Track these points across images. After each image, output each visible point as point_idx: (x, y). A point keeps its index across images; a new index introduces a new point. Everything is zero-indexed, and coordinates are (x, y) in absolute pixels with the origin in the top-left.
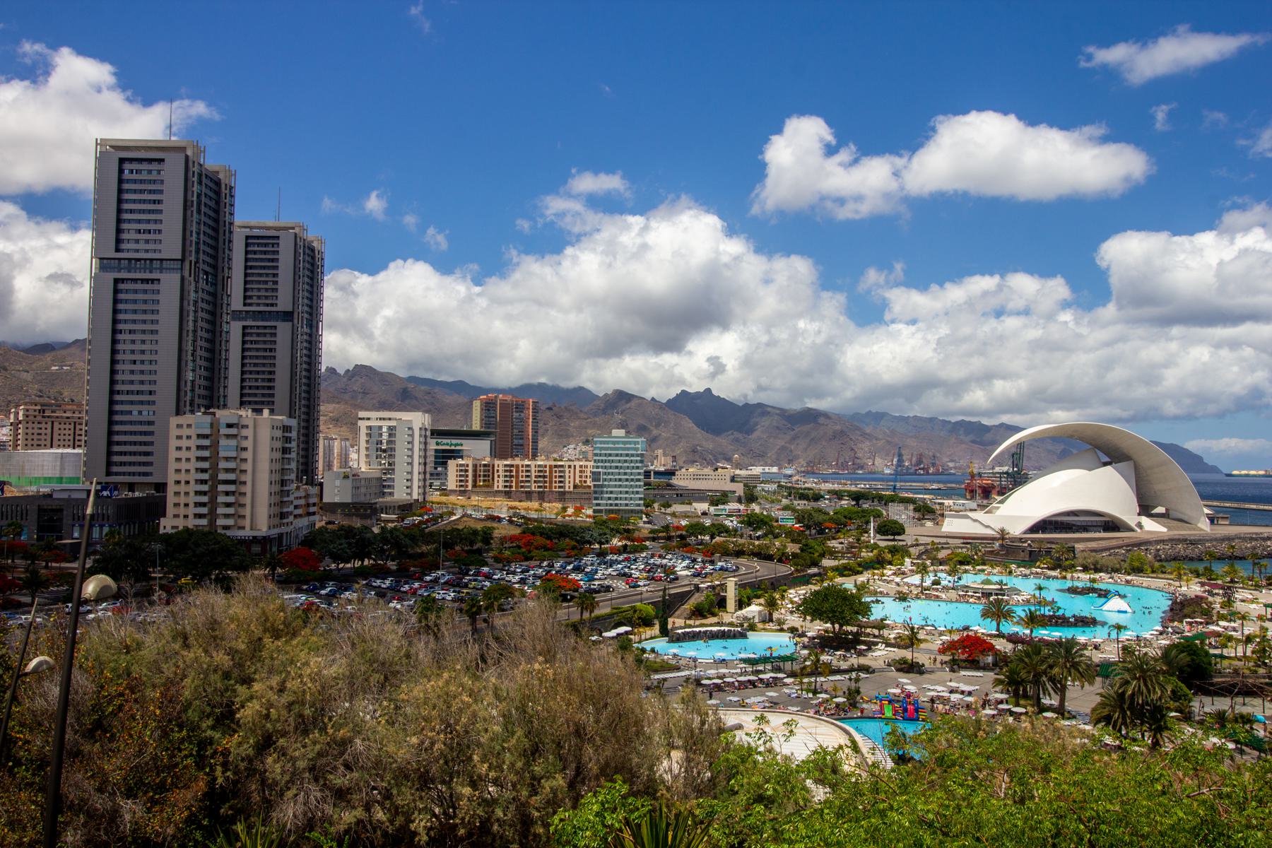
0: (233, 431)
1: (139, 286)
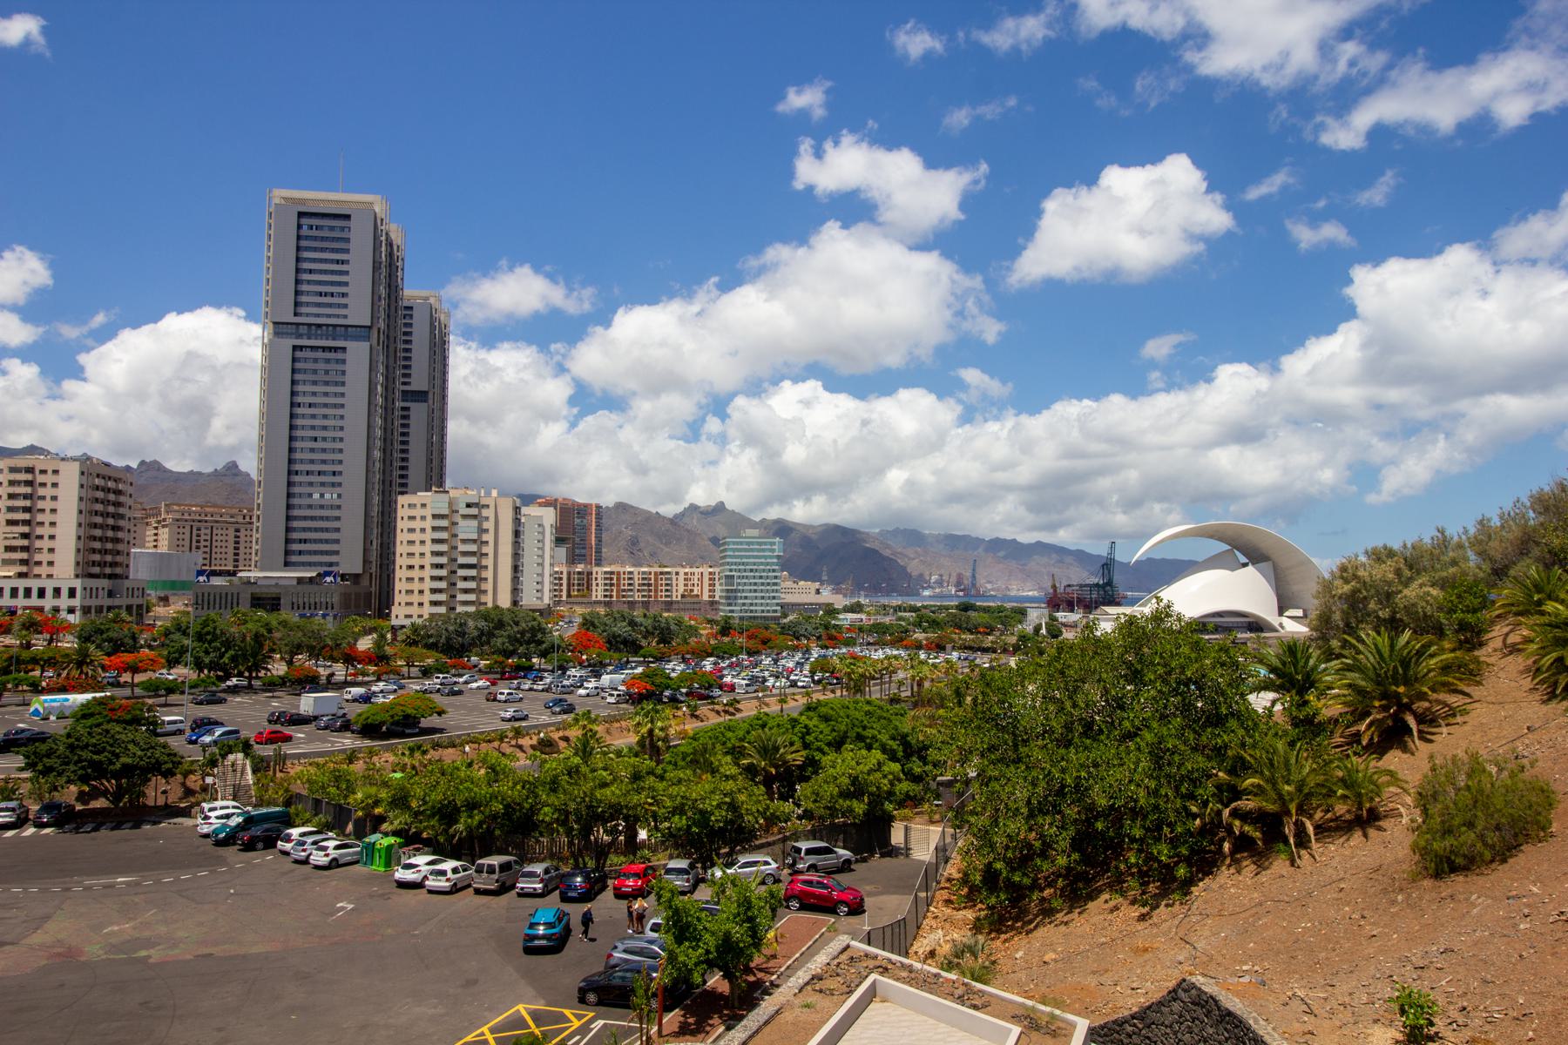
0: (474, 511)
1: (320, 354)
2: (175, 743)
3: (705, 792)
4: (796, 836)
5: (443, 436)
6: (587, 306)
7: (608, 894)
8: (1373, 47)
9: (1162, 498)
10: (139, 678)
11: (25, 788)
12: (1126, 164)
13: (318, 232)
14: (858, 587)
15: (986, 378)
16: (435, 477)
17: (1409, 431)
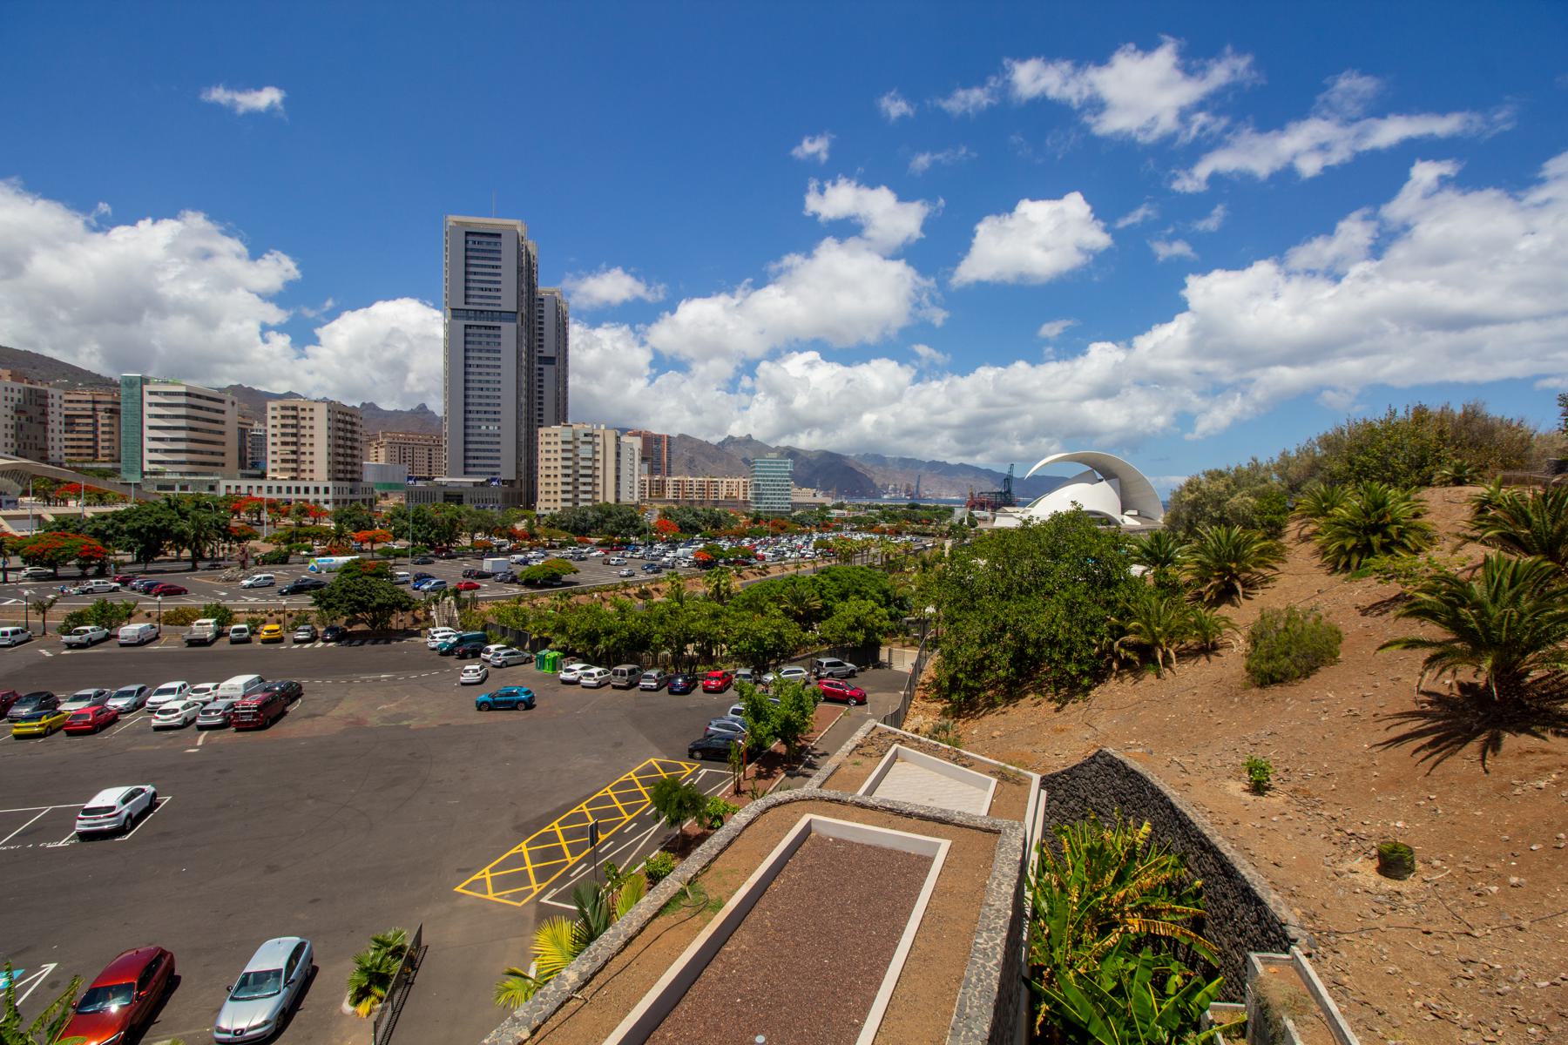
1: (483, 331)
2: (407, 588)
3: (763, 626)
4: (818, 655)
5: (566, 388)
6: (661, 296)
7: (699, 691)
8: (1217, 113)
9: (1048, 434)
10: (376, 547)
11: (313, 618)
12: (1033, 199)
13: (479, 246)
14: (840, 493)
15: (933, 352)
16: (561, 416)
17: (1215, 390)
